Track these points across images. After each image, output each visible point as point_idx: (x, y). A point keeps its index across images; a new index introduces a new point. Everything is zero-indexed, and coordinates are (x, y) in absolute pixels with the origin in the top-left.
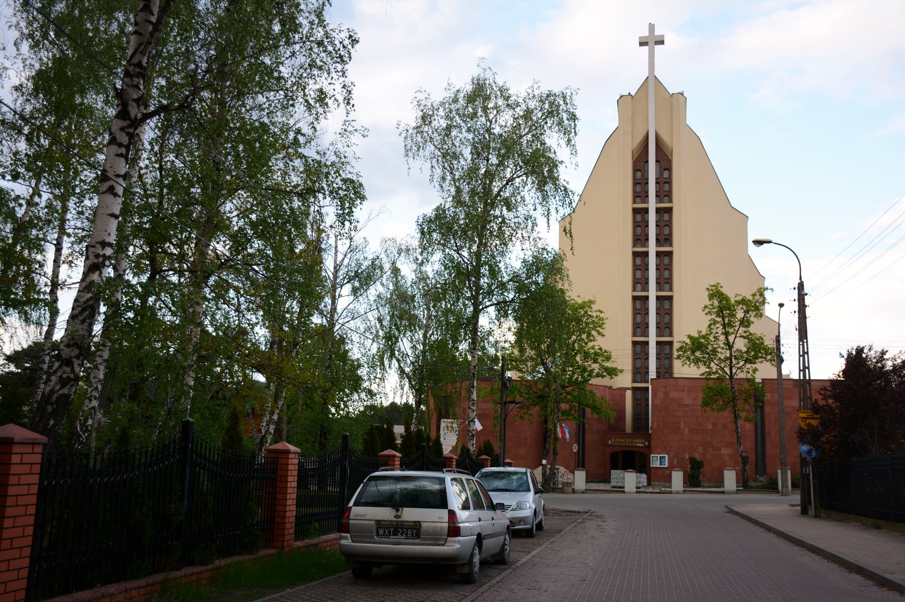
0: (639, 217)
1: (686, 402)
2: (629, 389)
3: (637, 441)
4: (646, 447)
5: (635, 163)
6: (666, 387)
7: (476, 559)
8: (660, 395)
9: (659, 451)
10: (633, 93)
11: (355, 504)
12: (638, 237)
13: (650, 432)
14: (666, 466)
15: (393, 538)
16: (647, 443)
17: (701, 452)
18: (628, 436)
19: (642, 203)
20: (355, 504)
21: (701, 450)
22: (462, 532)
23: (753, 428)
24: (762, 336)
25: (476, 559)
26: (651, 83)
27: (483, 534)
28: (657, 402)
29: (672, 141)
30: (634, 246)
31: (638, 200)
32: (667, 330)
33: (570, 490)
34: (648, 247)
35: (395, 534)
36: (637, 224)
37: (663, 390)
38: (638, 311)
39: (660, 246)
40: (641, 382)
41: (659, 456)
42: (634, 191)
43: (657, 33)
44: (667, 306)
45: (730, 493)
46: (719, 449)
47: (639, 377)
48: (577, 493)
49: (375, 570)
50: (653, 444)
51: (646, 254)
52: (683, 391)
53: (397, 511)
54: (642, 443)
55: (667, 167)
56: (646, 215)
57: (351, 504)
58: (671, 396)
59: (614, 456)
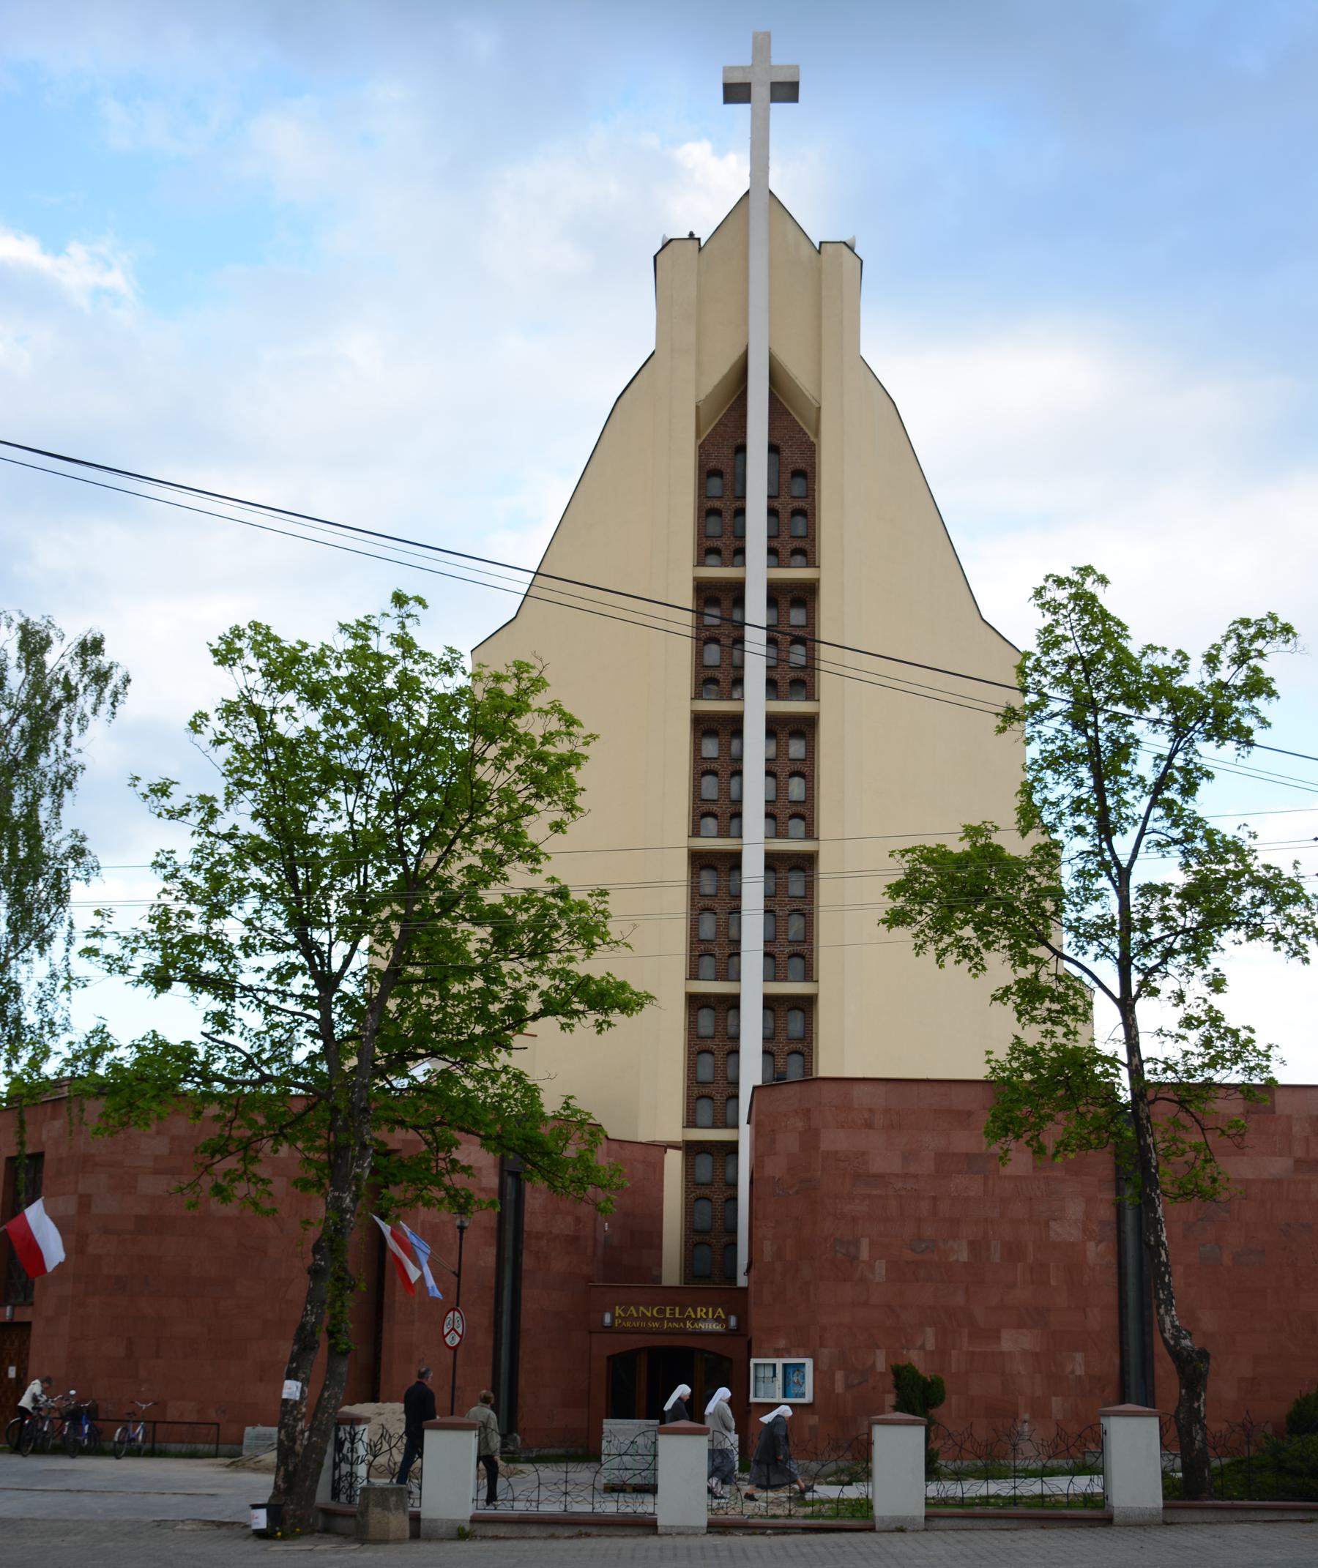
0: (710, 748)
1: (877, 1166)
2: (674, 1146)
3: (700, 1312)
4: (730, 1333)
5: (704, 450)
6: (808, 1111)
8: (788, 1143)
9: (782, 1343)
10: (704, 235)
12: (709, 673)
13: (742, 1281)
14: (808, 1398)
16: (733, 1321)
17: (930, 1345)
19: (720, 835)
21: (930, 1339)
23: (1111, 1259)
24: (1243, 834)
26: (758, 208)
28: (775, 1168)
29: (820, 395)
30: (697, 695)
31: (710, 824)
32: (797, 963)
33: (398, 1522)
34: (741, 699)
36: (704, 635)
37: (800, 1124)
38: (707, 903)
39: (778, 698)
40: (714, 1126)
41: (779, 1362)
42: (699, 664)
43: (777, 60)
44: (796, 887)
45: (1140, 1523)
46: (995, 1335)
47: (705, 1109)
48: (429, 1539)
50: (757, 1319)
51: (733, 861)
52: (869, 1125)
54: (718, 1320)
55: (802, 466)
56: (735, 743)
58: (825, 1145)
59: (621, 1365)
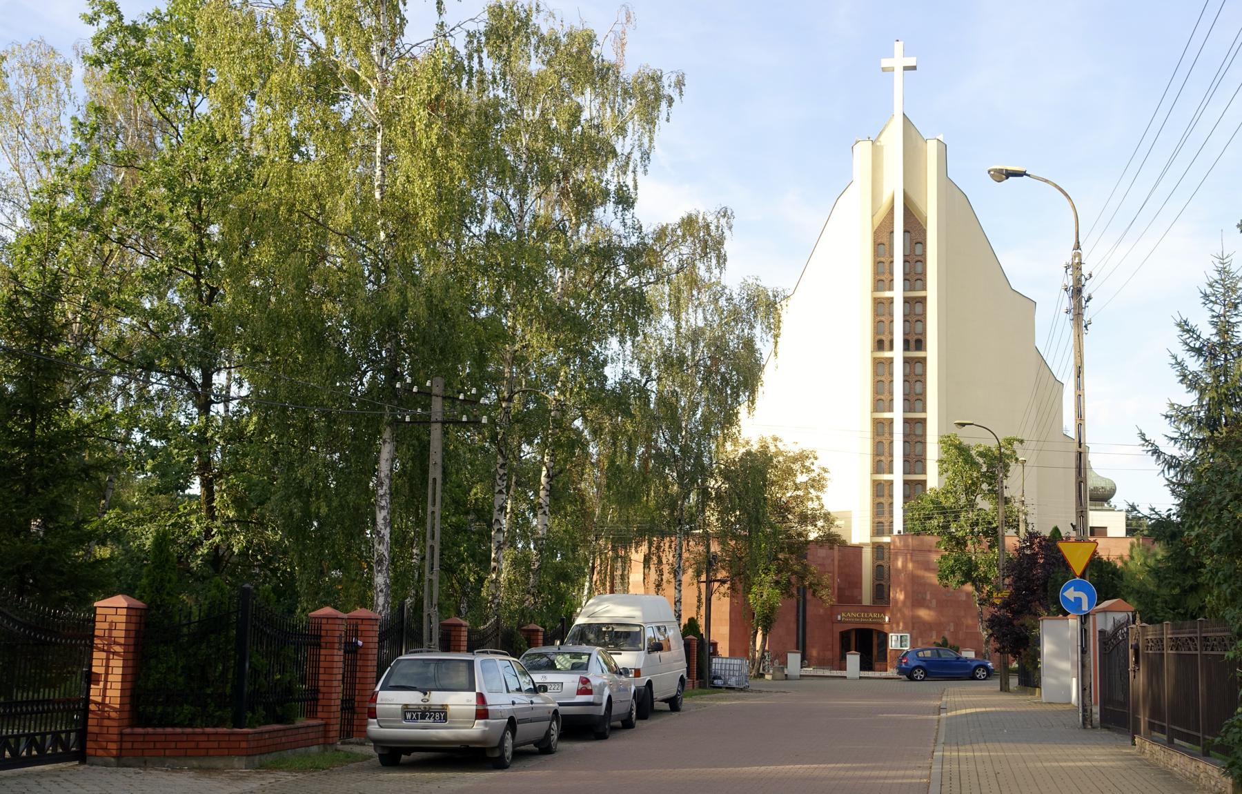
5: (876, 233)
7: (508, 744)
11: (381, 689)
15: (420, 723)
17: (952, 629)
18: (866, 609)
20: (381, 689)
22: (490, 715)
25: (508, 744)
27: (518, 717)
35: (423, 717)
49: (404, 758)
51: (907, 345)
53: (425, 694)
55: (920, 240)
57: (378, 689)
59: (845, 636)
